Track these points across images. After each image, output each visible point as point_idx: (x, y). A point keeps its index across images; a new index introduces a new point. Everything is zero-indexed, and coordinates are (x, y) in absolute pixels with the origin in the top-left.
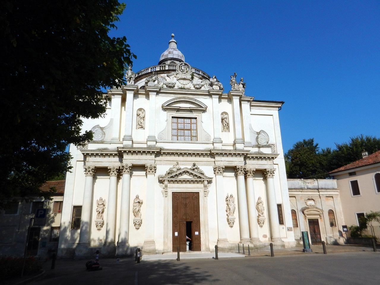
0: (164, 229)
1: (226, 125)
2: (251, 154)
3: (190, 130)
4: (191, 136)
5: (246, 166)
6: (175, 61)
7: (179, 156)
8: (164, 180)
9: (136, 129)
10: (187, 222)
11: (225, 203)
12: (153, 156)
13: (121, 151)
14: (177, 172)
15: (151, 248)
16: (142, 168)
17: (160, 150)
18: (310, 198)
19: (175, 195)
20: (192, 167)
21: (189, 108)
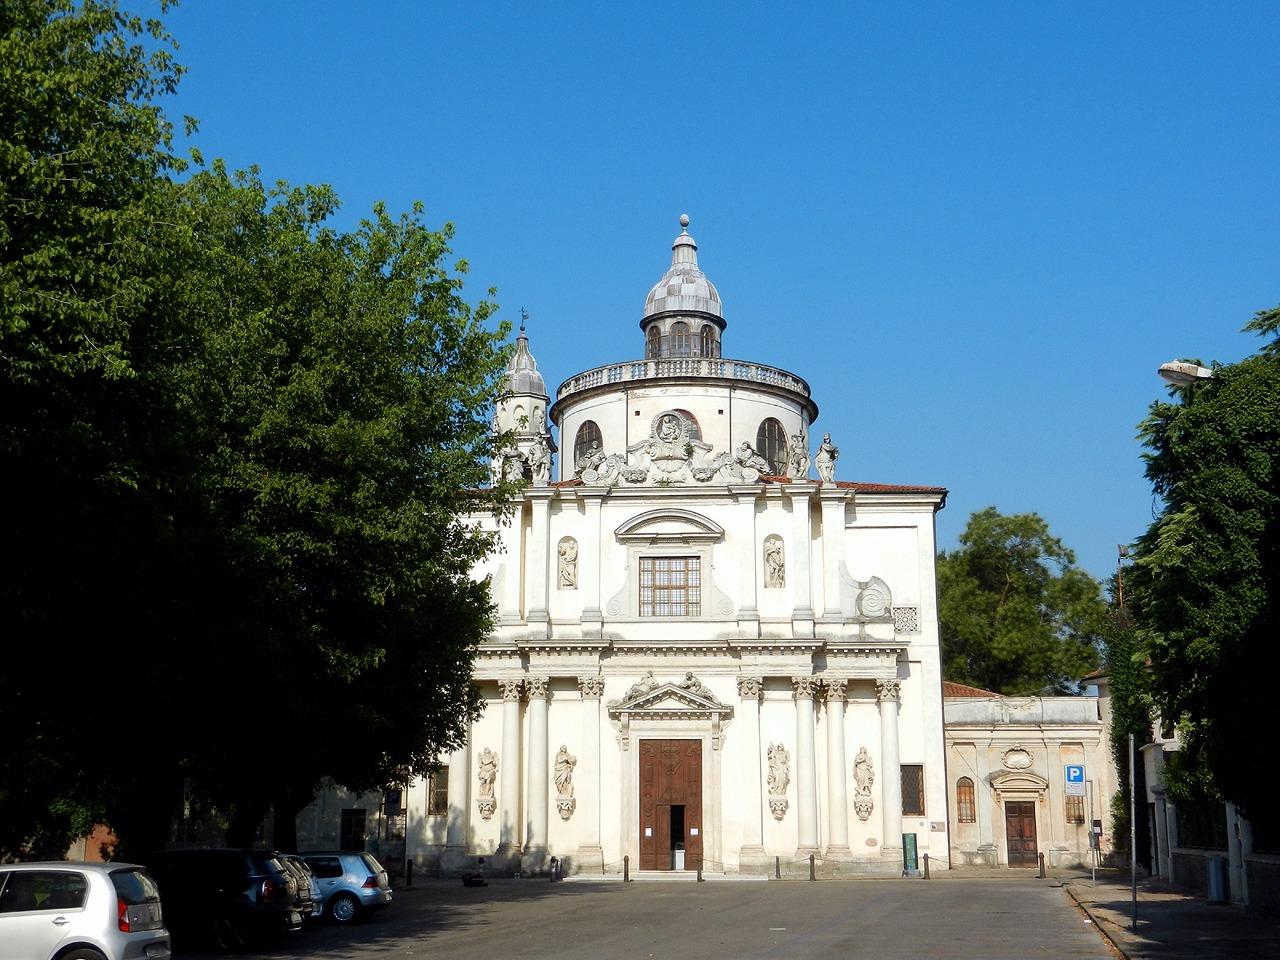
0: (622, 821)
2: (835, 643)
3: (685, 587)
4: (688, 603)
5: (828, 672)
6: (686, 320)
8: (620, 713)
9: (558, 588)
12: (596, 657)
13: (524, 648)
15: (595, 859)
16: (572, 683)
17: (611, 644)
18: (1017, 746)
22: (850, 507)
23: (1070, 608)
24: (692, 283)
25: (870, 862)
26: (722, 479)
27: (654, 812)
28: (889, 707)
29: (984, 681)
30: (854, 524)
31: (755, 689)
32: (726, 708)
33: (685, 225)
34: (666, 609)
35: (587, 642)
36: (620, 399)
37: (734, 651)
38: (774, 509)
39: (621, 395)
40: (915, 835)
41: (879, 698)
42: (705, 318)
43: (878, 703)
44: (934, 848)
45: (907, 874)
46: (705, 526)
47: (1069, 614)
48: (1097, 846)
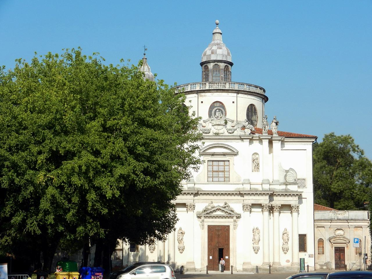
1: (256, 165)
2: (277, 192)
3: (224, 171)
4: (225, 177)
5: (274, 202)
6: (218, 64)
7: (213, 195)
8: (201, 216)
10: (219, 249)
11: (253, 234)
12: (192, 196)
14: (211, 209)
15: (192, 267)
17: (198, 192)
18: (339, 228)
19: (209, 227)
20: (224, 205)
21: (222, 153)
22: (283, 142)
23: (361, 173)
24: (221, 49)
25: (288, 268)
26: (238, 132)
27: (213, 250)
28: (295, 214)
29: (328, 200)
30: (284, 149)
31: (249, 208)
32: (239, 214)
33: (217, 24)
34: (217, 179)
35: (189, 191)
36: (195, 97)
37: (241, 195)
38: (256, 143)
39: (196, 95)
40: (304, 258)
41: (292, 211)
42: (226, 63)
43: (291, 213)
44: (310, 262)
45: (301, 272)
46: (231, 150)
47: (361, 175)
48: (366, 263)
